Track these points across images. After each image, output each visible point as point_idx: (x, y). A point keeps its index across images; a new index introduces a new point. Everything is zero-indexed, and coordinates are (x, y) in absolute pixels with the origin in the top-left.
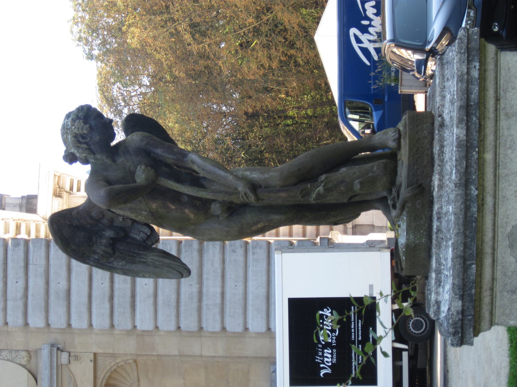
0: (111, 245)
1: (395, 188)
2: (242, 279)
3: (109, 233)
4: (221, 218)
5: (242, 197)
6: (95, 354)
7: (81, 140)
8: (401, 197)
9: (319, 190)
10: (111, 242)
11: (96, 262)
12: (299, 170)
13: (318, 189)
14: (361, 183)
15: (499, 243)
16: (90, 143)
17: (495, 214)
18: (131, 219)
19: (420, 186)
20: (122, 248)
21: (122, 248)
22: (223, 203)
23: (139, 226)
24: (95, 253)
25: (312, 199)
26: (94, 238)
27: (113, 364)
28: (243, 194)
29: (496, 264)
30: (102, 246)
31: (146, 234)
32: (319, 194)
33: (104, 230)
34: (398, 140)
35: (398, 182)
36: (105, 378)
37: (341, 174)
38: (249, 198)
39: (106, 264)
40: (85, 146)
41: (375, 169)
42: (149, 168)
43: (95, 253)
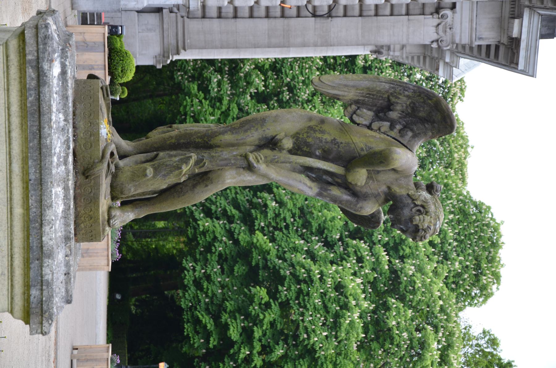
3: (394, 115)
4: (283, 134)
5: (261, 159)
7: (422, 209)
8: (106, 165)
10: (392, 107)
12: (207, 186)
13: (188, 168)
14: (146, 175)
15: (4, 102)
16: (412, 206)
17: (10, 153)
18: (372, 130)
19: (87, 177)
20: (380, 102)
22: (281, 149)
24: (408, 97)
25: (193, 158)
26: (409, 111)
28: (261, 161)
29: (6, 105)
30: (400, 104)
31: (357, 115)
32: (187, 163)
33: (400, 118)
34: (110, 218)
35: (109, 178)
37: (166, 183)
38: (254, 156)
39: (396, 86)
40: (418, 203)
41: (132, 190)
42: (353, 183)
43: (408, 97)
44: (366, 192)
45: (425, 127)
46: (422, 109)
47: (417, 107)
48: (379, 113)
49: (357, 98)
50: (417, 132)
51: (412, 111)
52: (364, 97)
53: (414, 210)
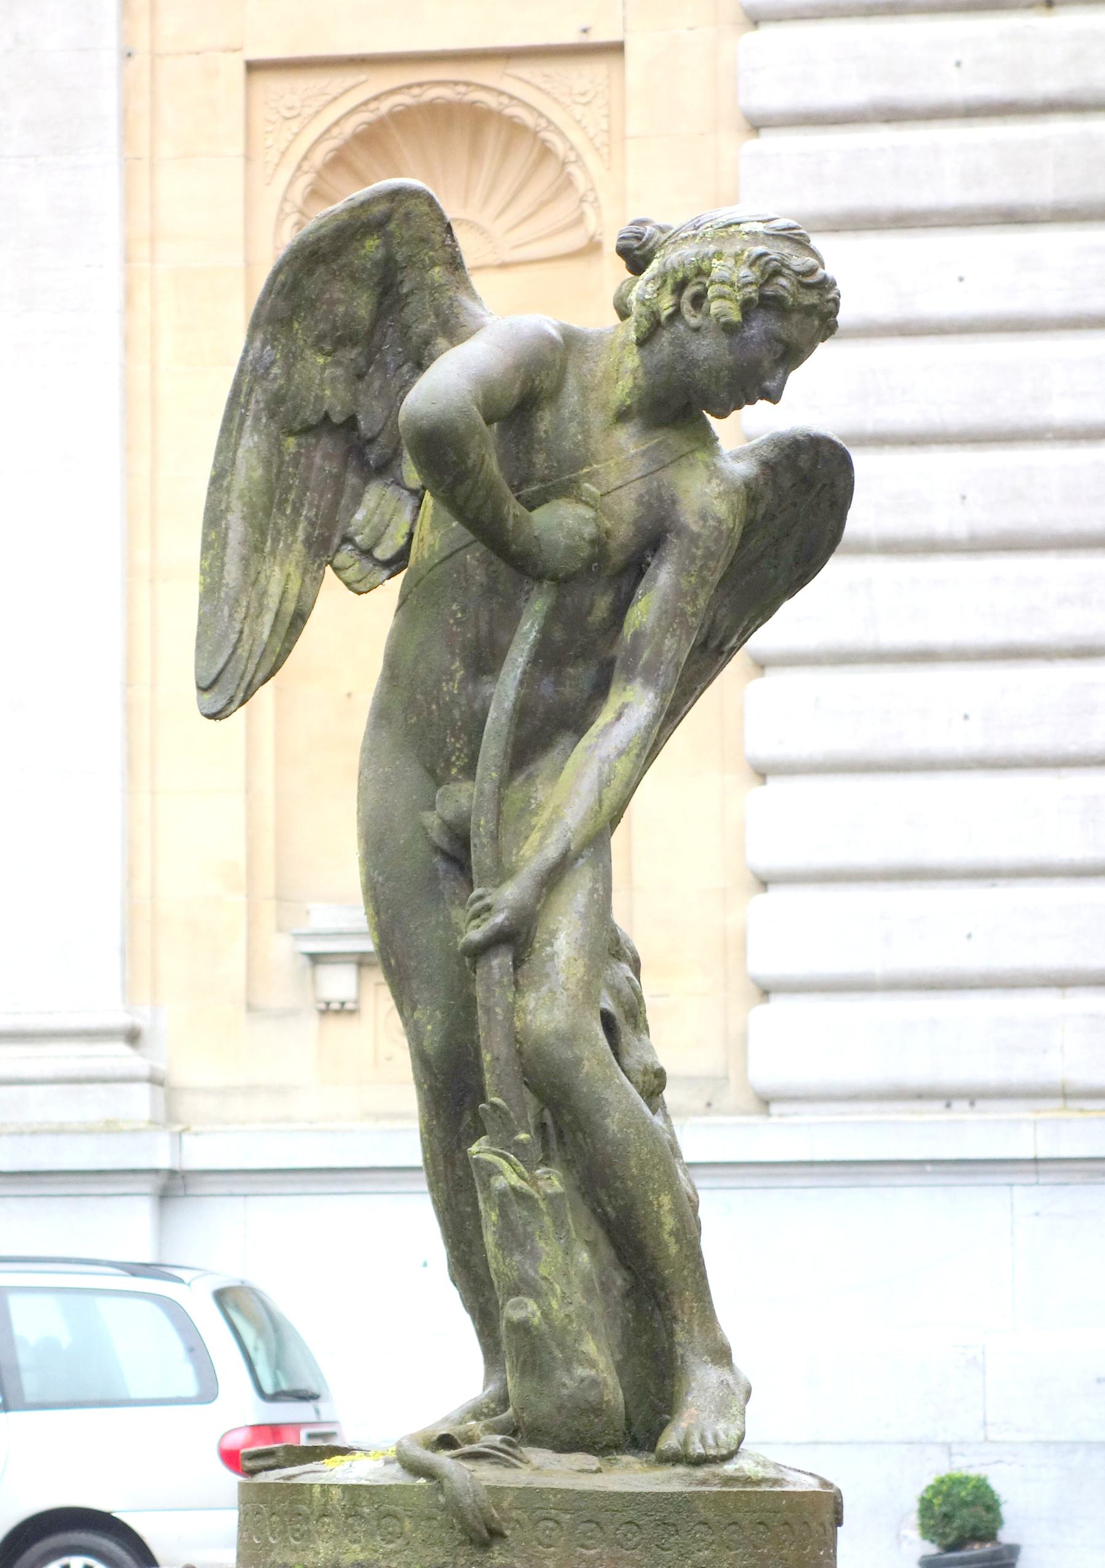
0: (327, 417)
1: (504, 1446)
2: (999, 744)
6: (616, 49)
9: (501, 1173)
11: (254, 369)
21: (318, 460)
23: (407, 516)
27: (575, 136)
28: (488, 900)
31: (377, 542)
36: (288, 208)
38: (474, 923)
44: (640, 501)
45: (411, 292)
46: (341, 309)
47: (335, 328)
48: (367, 463)
49: (299, 547)
50: (432, 319)
51: (355, 345)
52: (294, 525)
53: (693, 319)
